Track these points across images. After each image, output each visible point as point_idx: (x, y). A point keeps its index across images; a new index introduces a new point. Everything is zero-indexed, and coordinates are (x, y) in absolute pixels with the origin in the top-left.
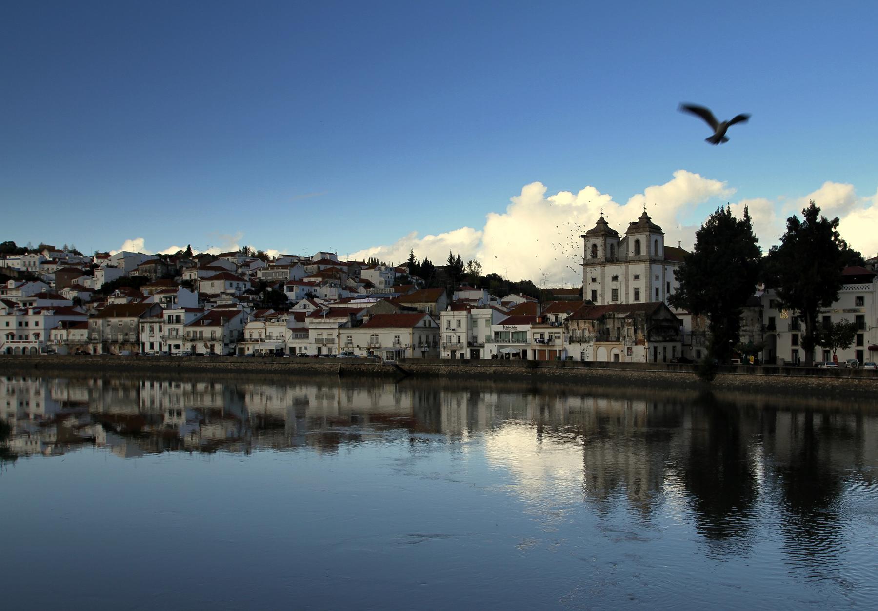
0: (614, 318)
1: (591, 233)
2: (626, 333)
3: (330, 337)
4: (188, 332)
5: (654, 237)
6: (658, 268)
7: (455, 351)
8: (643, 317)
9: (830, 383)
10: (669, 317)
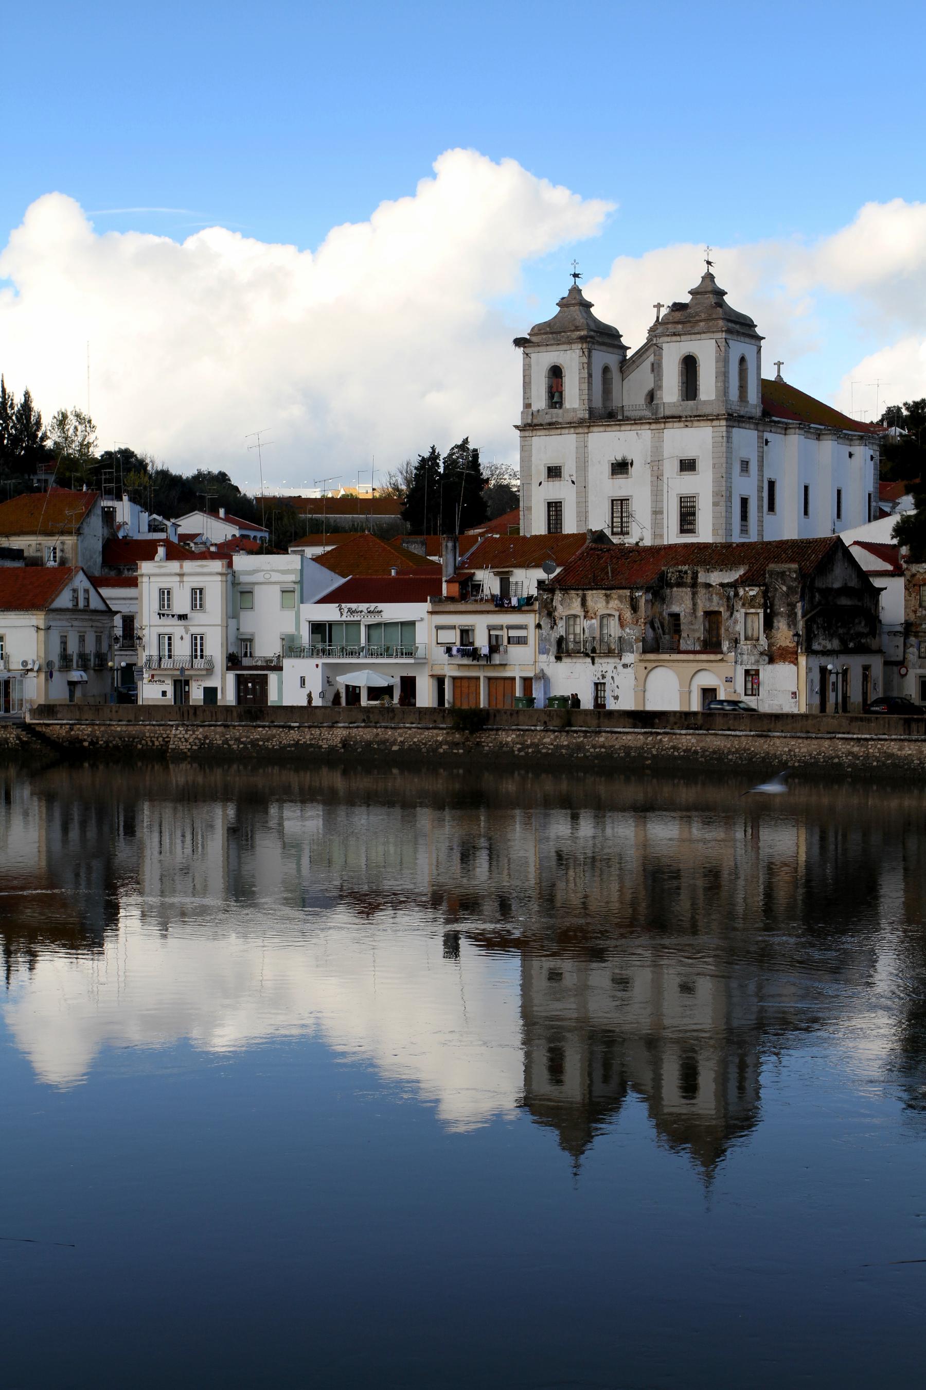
0: (694, 585)
1: (546, 333)
2: (740, 628)
5: (739, 347)
6: (746, 438)
7: (187, 683)
8: (795, 579)
10: (854, 583)
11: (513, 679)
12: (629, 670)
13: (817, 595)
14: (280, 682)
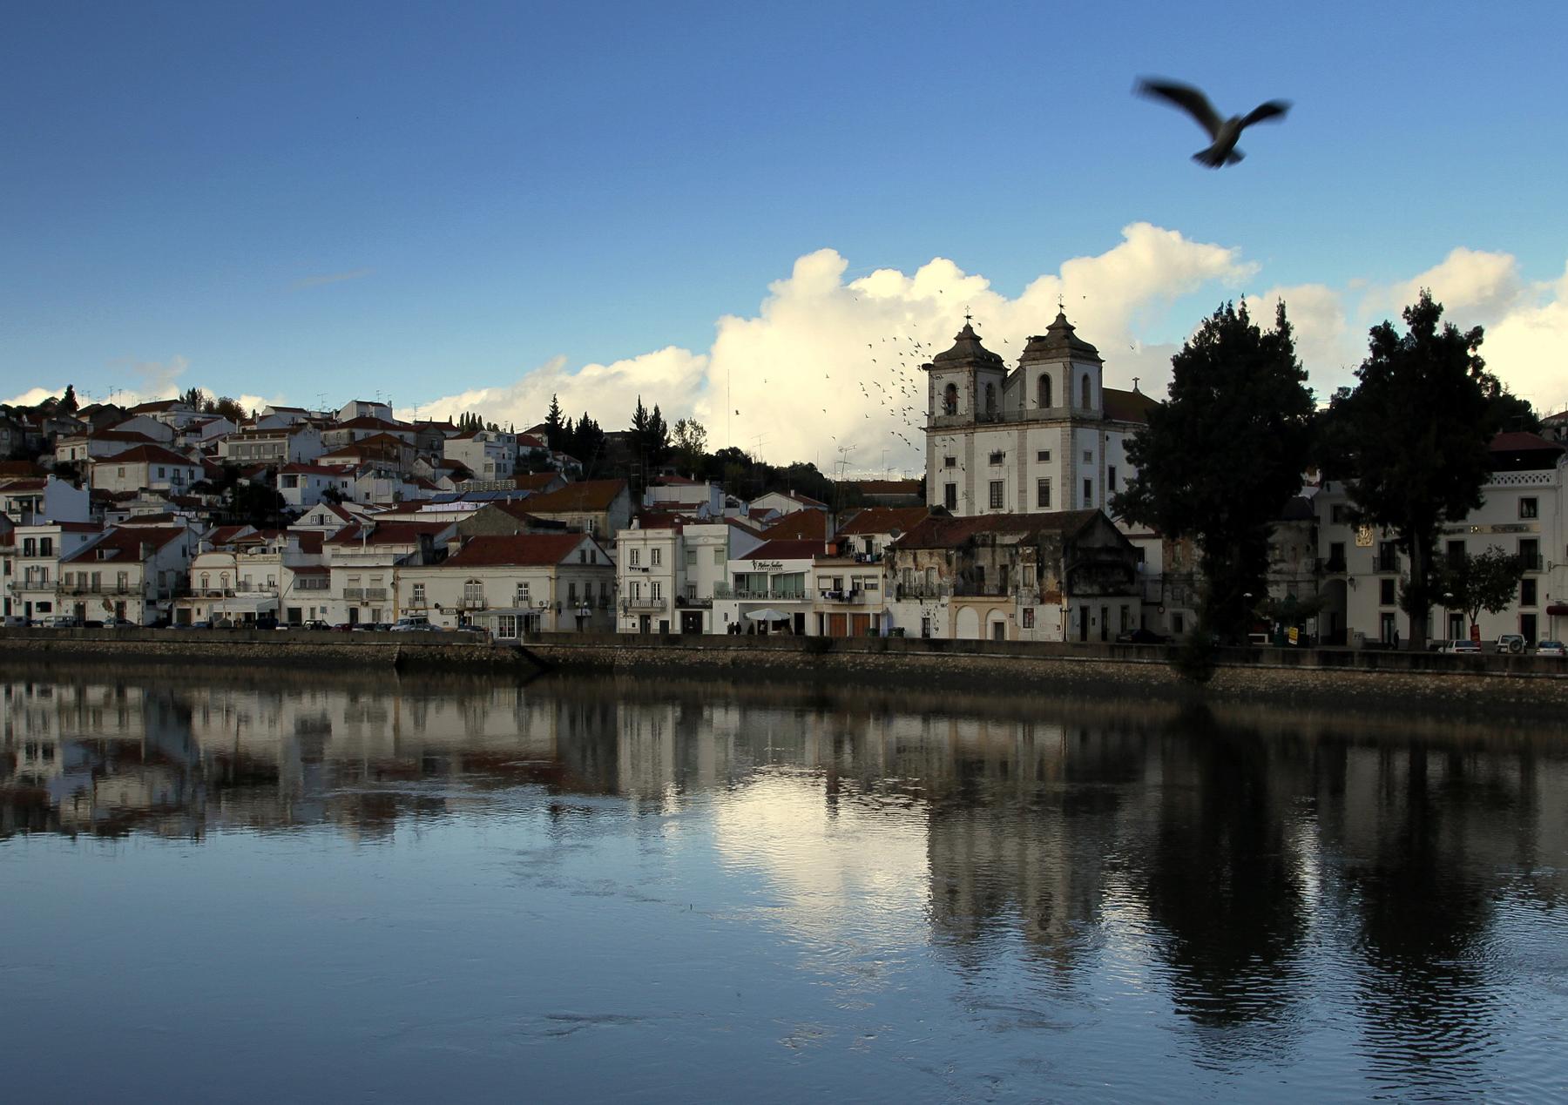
0: (993, 545)
1: (945, 360)
2: (1020, 577)
3: (377, 586)
4: (69, 576)
5: (1081, 368)
7: (648, 617)
9: (1464, 685)
10: (1114, 543)
11: (869, 615)
12: (945, 609)
13: (1079, 553)
14: (711, 617)
